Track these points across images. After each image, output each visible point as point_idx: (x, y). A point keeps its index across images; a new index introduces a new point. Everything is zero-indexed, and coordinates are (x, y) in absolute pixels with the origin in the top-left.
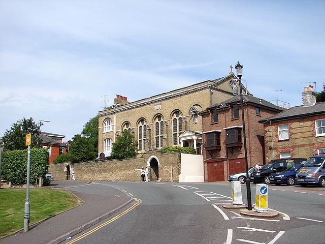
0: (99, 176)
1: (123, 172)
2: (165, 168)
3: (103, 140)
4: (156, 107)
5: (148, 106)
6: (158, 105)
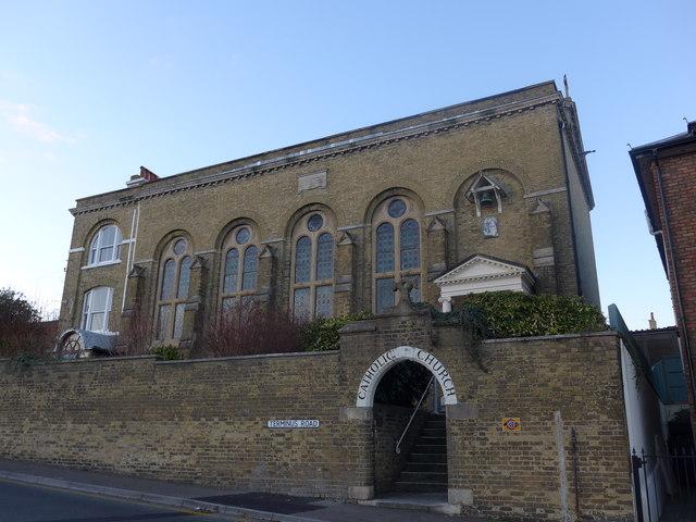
0: (42, 437)
1: (191, 428)
2: (505, 431)
3: (82, 290)
4: (305, 182)
5: (271, 179)
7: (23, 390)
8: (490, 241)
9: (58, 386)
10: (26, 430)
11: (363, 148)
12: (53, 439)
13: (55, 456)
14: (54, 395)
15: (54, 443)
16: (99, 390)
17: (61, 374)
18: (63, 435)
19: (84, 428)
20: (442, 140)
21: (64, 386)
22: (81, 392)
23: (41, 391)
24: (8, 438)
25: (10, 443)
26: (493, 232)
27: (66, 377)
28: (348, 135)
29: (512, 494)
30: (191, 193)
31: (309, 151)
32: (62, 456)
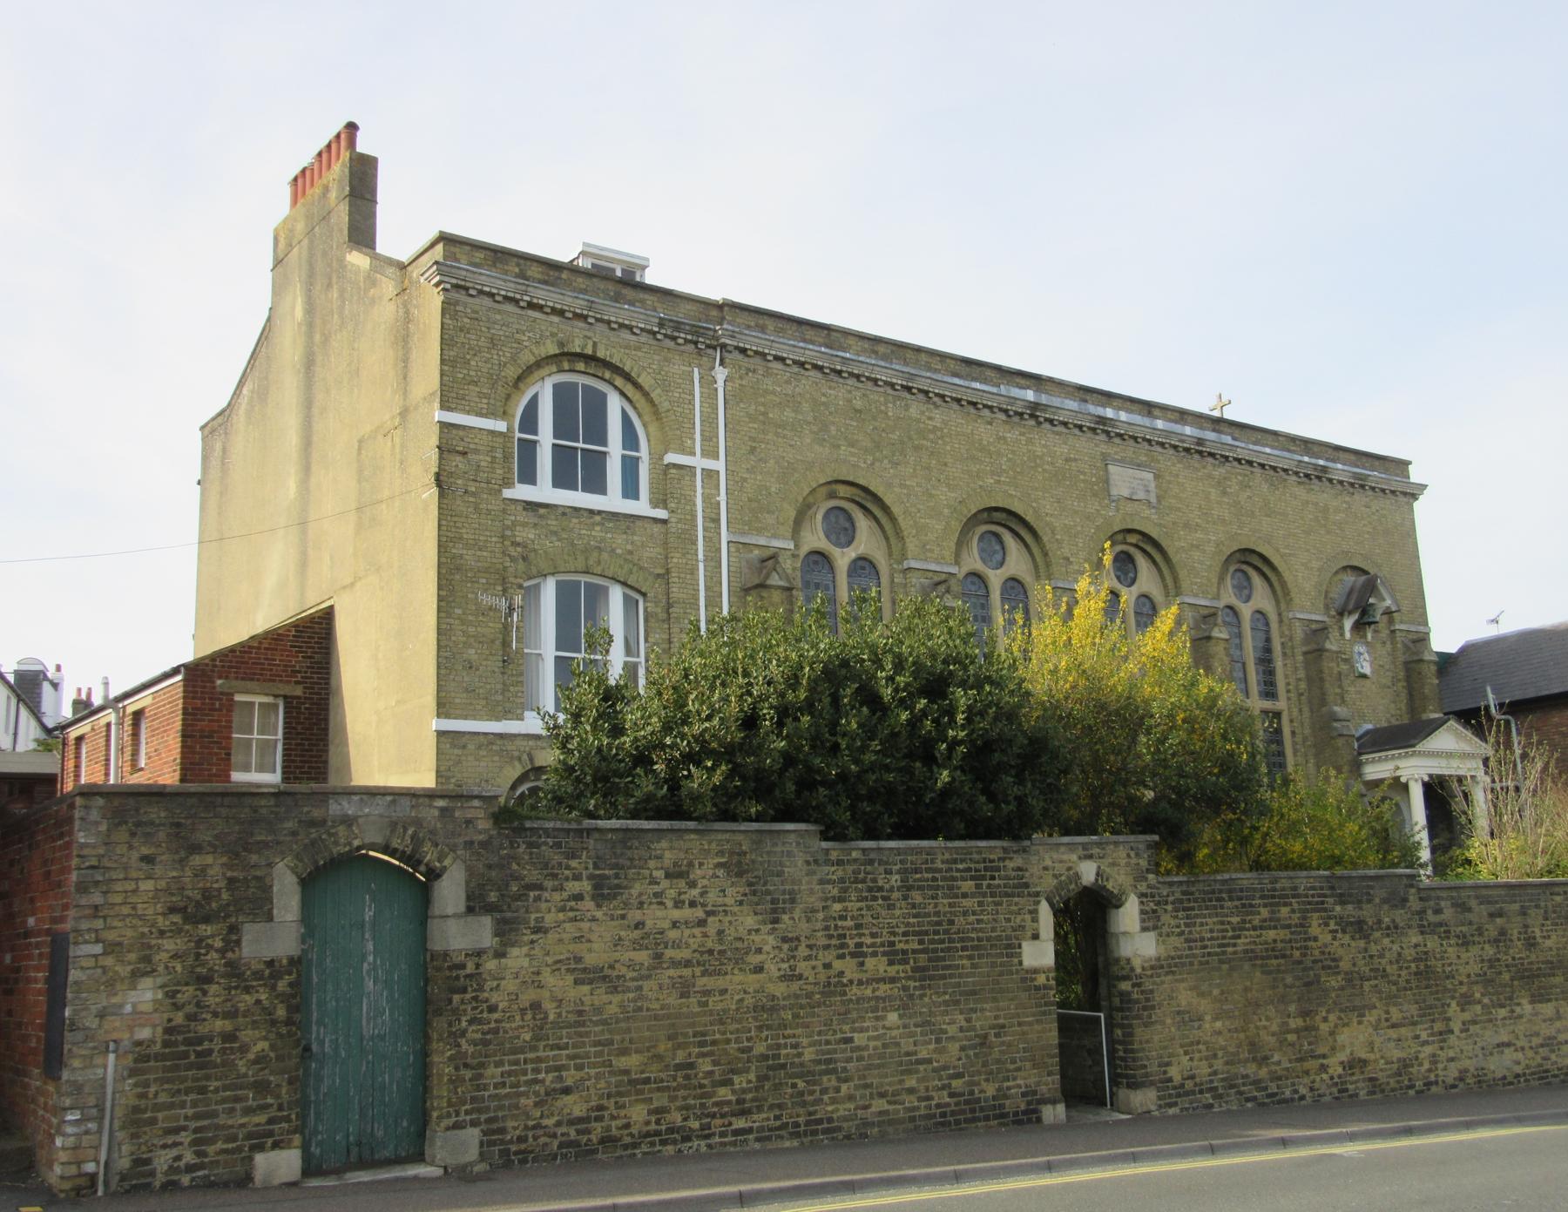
0: (1490, 1037)
8: (1361, 682)
9: (1492, 931)
10: (1456, 1026)
11: (1212, 455)
12: (1505, 1039)
13: (1518, 1069)
14: (1490, 951)
15: (1508, 1045)
16: (1554, 937)
17: (1492, 908)
18: (1521, 1028)
19: (1548, 1009)
20: (1301, 492)
21: (1503, 932)
22: (1531, 944)
23: (1465, 943)
24: (1428, 1050)
25: (1434, 1059)
27: (1500, 915)
28: (1108, 397)
29: (869, 1039)
30: (877, 395)
32: (1528, 1067)
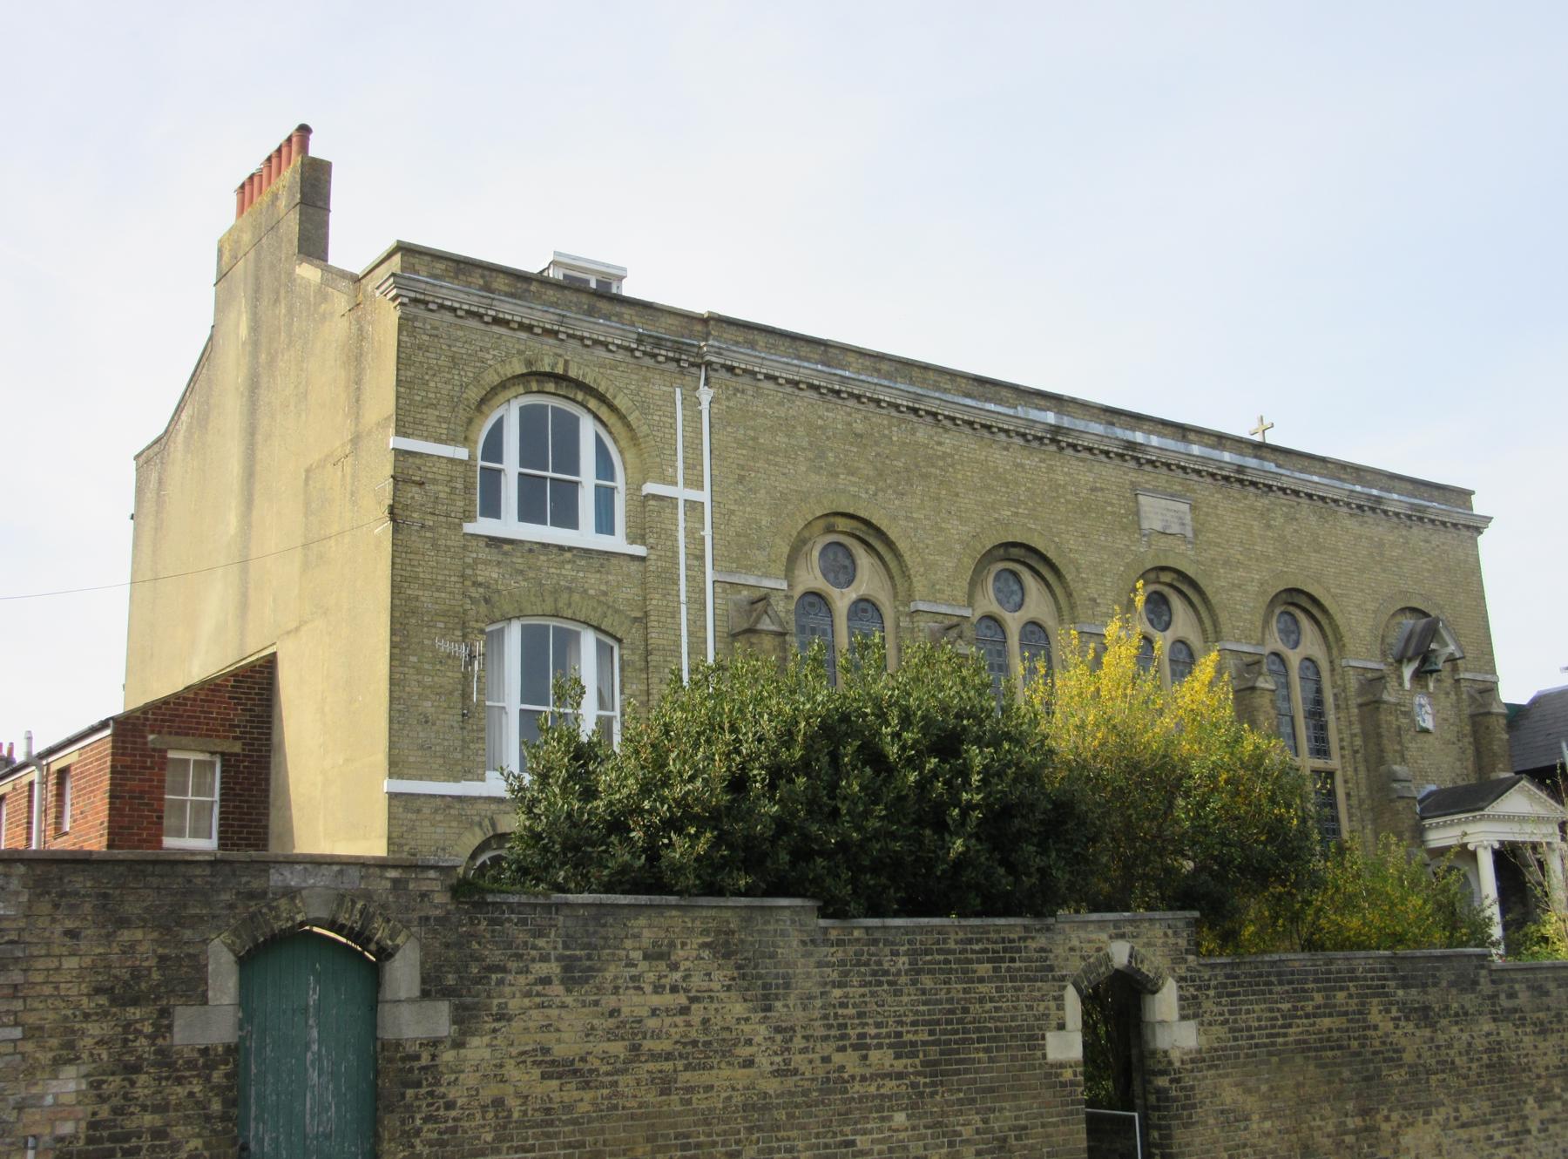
6: (1173, 496)
7: (1506, 1031)
10: (1534, 1126)
23: (1543, 1031)
26: (1429, 723)
31: (1196, 449)
